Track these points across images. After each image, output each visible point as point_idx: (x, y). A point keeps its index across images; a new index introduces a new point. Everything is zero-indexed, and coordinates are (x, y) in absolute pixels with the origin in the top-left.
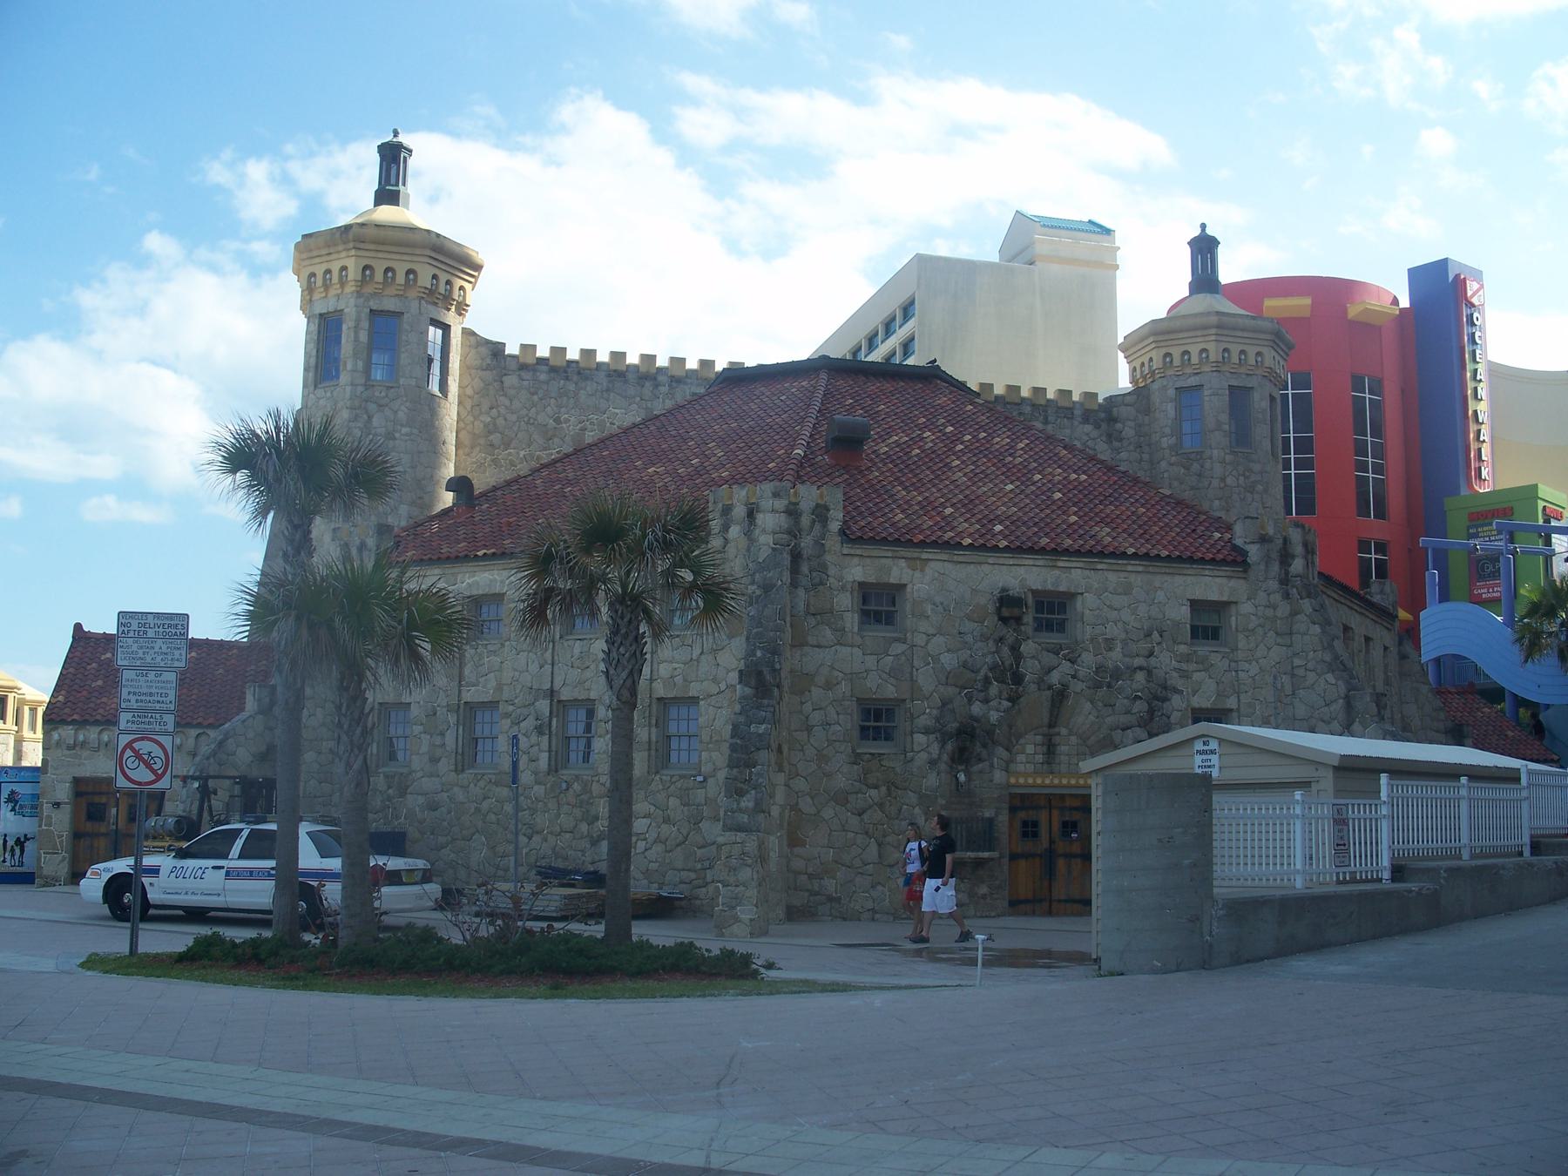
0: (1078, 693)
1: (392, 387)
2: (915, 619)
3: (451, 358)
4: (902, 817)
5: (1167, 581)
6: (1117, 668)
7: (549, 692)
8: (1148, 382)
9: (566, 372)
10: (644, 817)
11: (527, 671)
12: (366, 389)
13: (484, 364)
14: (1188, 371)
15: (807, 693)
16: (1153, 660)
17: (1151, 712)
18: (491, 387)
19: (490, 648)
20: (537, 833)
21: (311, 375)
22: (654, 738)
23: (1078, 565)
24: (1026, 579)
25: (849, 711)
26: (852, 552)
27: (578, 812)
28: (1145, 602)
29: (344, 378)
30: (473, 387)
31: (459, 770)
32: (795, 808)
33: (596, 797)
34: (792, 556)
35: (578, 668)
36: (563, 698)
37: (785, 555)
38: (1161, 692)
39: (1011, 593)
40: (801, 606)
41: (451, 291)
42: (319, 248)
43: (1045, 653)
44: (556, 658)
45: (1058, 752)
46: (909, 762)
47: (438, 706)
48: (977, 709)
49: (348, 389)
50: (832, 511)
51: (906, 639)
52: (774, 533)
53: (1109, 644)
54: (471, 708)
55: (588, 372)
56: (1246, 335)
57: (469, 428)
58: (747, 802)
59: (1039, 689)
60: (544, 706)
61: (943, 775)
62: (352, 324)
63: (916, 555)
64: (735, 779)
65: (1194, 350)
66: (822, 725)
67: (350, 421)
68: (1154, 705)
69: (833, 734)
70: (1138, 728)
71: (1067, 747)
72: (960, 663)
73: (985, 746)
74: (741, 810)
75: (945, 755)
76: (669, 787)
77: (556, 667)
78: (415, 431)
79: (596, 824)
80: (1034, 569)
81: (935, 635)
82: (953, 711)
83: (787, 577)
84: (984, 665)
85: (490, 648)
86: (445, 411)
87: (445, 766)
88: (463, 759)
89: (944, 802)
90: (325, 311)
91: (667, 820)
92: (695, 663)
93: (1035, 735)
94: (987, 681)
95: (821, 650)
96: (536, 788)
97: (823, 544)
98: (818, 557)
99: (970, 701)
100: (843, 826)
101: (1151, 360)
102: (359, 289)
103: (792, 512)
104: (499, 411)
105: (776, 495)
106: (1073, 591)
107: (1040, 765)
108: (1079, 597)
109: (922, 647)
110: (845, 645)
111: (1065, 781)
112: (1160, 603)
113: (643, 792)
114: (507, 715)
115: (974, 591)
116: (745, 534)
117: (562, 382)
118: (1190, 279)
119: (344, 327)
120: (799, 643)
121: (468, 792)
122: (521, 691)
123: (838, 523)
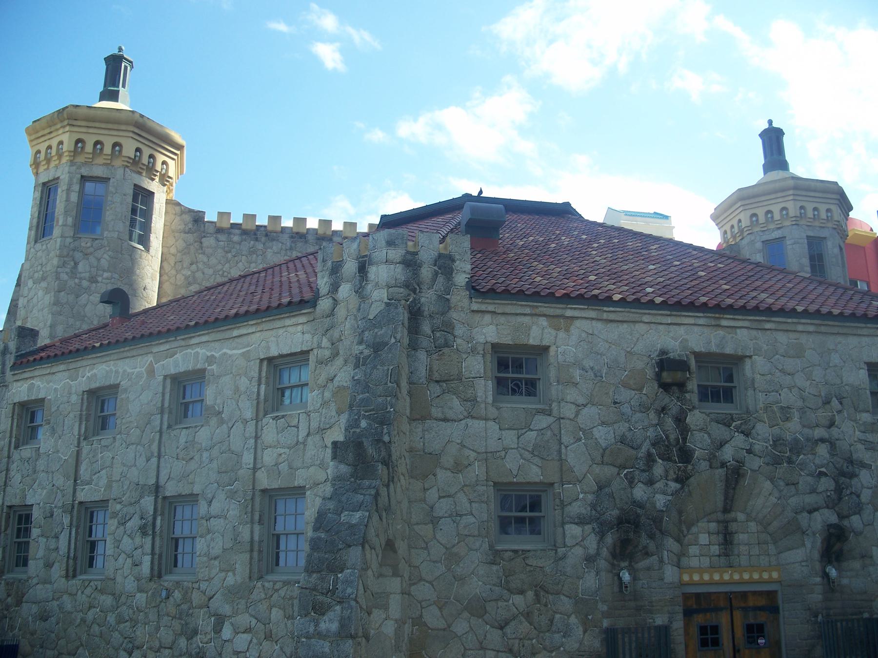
0: (756, 471)
1: (96, 239)
2: (560, 386)
3: (154, 219)
4: (554, 629)
5: (840, 343)
6: (796, 440)
7: (153, 489)
8: (737, 241)
9: (255, 234)
10: (244, 633)
11: (136, 466)
12: (74, 241)
13: (187, 228)
14: (772, 226)
15: (431, 476)
16: (834, 431)
17: (839, 490)
18: (192, 247)
19: (103, 443)
20: (138, 648)
21: (33, 232)
22: (256, 538)
23: (746, 324)
24: (687, 341)
25: (485, 498)
26: (483, 307)
27: (177, 625)
28: (819, 365)
29: (57, 232)
30: (176, 247)
31: (71, 574)
32: (418, 621)
33: (196, 608)
34: (410, 312)
35: (183, 459)
36: (168, 494)
37: (401, 310)
38: (847, 467)
39: (671, 355)
40: (422, 372)
41: (154, 164)
42: (44, 129)
43: (714, 424)
44: (163, 449)
45: (735, 542)
46: (561, 559)
47: (55, 507)
48: (640, 492)
49: (59, 240)
50: (458, 262)
51: (551, 410)
52: (389, 287)
53: (786, 412)
54: (87, 508)
55: (275, 234)
56: (817, 194)
57: (172, 280)
58: (329, 623)
59: (711, 467)
60: (148, 502)
61: (603, 574)
62: (65, 187)
63: (558, 312)
64: (314, 589)
65: (776, 209)
66: (450, 516)
67: (58, 267)
68: (841, 482)
69: (465, 527)
70: (826, 510)
71: (746, 536)
72: (618, 437)
73: (651, 537)
74: (320, 635)
75: (605, 549)
76: (272, 596)
77: (162, 460)
78: (116, 276)
79: (195, 639)
80: (696, 329)
81: (585, 406)
82: (611, 495)
83: (402, 334)
84: (645, 440)
85: (103, 443)
86: (146, 263)
87: (57, 571)
88: (75, 564)
89: (605, 608)
90: (46, 180)
91: (269, 636)
92: (302, 446)
93: (709, 522)
94: (650, 460)
95: (449, 424)
96: (138, 595)
97: (448, 300)
98: (442, 314)
99: (631, 482)
100: (481, 643)
101: (740, 221)
102: (72, 158)
103: (411, 262)
104: (197, 266)
105: (390, 243)
106: (740, 353)
107: (717, 558)
108: (748, 361)
109: (571, 420)
110: (477, 418)
111: (746, 576)
112: (836, 366)
113: (243, 602)
114: (115, 515)
115: (629, 353)
116: (356, 292)
117: (252, 242)
118: (763, 162)
119: (59, 190)
120: (420, 415)
121: (76, 601)
122: (128, 488)
123: (465, 276)
